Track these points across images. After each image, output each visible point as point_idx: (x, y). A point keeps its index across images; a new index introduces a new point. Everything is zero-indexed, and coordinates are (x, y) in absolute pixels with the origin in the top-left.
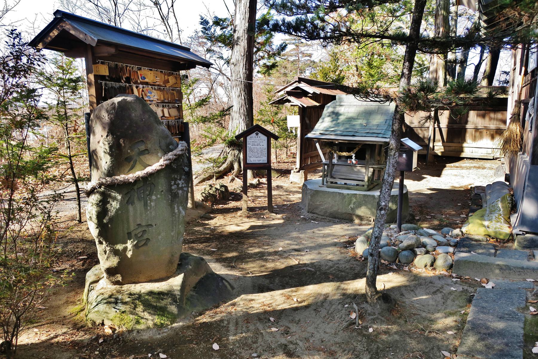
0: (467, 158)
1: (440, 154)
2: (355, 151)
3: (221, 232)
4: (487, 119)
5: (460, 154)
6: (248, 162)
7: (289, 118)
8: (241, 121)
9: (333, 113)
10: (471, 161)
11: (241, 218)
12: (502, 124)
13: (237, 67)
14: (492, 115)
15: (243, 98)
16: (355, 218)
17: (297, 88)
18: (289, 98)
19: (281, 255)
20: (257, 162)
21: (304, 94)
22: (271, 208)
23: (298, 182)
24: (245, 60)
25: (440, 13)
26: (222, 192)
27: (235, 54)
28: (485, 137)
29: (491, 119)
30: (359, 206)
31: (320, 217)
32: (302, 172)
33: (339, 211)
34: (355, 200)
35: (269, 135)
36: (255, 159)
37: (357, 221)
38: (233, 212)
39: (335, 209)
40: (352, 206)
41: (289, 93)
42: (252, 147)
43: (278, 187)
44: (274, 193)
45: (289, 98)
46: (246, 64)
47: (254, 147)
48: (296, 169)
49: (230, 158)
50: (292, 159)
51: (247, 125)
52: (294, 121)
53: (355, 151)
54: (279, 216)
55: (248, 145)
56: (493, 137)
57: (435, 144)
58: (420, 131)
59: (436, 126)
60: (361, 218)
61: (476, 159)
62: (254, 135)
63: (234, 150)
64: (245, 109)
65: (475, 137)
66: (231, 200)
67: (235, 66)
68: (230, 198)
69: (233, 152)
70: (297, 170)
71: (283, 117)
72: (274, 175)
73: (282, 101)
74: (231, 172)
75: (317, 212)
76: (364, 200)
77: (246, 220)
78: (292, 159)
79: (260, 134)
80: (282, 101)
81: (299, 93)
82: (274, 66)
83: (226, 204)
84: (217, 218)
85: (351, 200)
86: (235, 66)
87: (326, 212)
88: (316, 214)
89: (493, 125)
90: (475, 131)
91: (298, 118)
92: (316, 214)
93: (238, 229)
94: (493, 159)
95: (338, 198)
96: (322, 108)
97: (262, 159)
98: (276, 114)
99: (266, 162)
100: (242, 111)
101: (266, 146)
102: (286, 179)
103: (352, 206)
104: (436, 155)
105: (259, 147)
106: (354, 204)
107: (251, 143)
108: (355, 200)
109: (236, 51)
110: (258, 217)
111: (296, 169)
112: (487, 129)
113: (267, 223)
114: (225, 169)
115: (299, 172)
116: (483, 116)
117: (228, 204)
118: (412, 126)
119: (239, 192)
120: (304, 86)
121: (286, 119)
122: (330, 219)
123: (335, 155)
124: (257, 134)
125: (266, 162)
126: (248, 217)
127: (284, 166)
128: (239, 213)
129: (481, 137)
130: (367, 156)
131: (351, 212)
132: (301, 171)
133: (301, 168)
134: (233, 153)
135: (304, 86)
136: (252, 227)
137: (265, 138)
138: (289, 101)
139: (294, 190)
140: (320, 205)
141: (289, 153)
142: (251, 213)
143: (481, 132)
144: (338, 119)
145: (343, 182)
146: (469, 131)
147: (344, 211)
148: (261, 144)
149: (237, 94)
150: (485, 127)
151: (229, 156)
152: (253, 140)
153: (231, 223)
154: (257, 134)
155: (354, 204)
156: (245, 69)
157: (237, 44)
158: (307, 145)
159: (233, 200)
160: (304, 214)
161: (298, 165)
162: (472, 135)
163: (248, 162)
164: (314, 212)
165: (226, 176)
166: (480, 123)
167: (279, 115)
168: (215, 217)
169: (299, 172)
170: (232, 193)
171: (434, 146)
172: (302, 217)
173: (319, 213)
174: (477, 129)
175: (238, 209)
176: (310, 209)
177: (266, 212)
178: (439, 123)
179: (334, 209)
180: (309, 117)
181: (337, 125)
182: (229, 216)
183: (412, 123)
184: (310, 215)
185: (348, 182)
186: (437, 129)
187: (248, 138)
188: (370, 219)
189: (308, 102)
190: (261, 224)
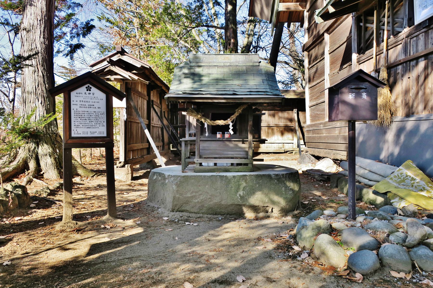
0: (263, 153)
2: (234, 117)
3: (30, 271)
4: (276, 117)
5: (258, 150)
6: (73, 135)
8: (38, 104)
10: (267, 155)
11: (65, 234)
12: (289, 122)
13: (31, 34)
14: (280, 114)
15: (40, 74)
16: (245, 209)
20: (89, 135)
22: (114, 210)
23: (124, 180)
24: (43, 26)
25: (230, 26)
26: (18, 196)
27: (29, 16)
28: (276, 134)
29: (280, 118)
30: (252, 192)
31: (193, 215)
32: (127, 166)
33: (223, 203)
34: (244, 184)
36: (86, 130)
37: (249, 214)
38: (44, 225)
39: (216, 200)
40: (241, 193)
42: (79, 109)
44: (201, 151)
46: (44, 32)
47: (83, 109)
48: (120, 163)
49: (22, 154)
53: (234, 117)
54: (130, 222)
55: (72, 107)
56: (282, 134)
60: (255, 209)
61: (271, 153)
62: (83, 89)
63: (27, 143)
64: (44, 89)
65: (268, 133)
66: (34, 208)
67: (28, 32)
68: (32, 205)
69: (27, 146)
70: (122, 164)
74: (24, 172)
75: (188, 208)
76: (258, 183)
79: (94, 89)
82: (79, 46)
83: (28, 215)
84: (15, 240)
85: (239, 185)
86: (28, 32)
87: (203, 206)
88: (186, 211)
89: (282, 123)
90: (268, 129)
92: (186, 211)
93: (67, 256)
94: (284, 153)
95: (219, 184)
97: (97, 130)
99: (105, 135)
100: (39, 92)
103: (241, 193)
105: (92, 110)
106: (243, 190)
107: (78, 103)
108: (244, 184)
109: (29, 14)
110: (98, 229)
111: (120, 163)
112: (277, 126)
113: (117, 236)
114: (14, 169)
116: (274, 116)
117: (31, 214)
119: (44, 195)
122: (209, 216)
124: (89, 89)
125: (105, 135)
126: (79, 230)
128: (58, 226)
129: (273, 133)
131: (241, 202)
132: (126, 166)
133: (126, 162)
134: (27, 147)
136: (94, 249)
139: (125, 188)
140: (192, 197)
142: (80, 223)
143: (273, 129)
145: (211, 163)
146: (263, 128)
147: (230, 202)
148: (96, 105)
150: (276, 124)
151: (20, 151)
152: (82, 99)
153: (48, 246)
154: (89, 89)
155: (243, 190)
156: (44, 38)
157: (31, 5)
159: (38, 207)
160: (166, 214)
162: (266, 132)
163: (73, 135)
164: (183, 209)
165: (17, 178)
166: (271, 121)
168: (10, 240)
169: (123, 166)
170: (34, 198)
172: (166, 218)
173: (192, 210)
174: (269, 127)
176: (176, 205)
177: (108, 219)
179: (215, 201)
182: (39, 233)
184: (178, 215)
185: (218, 161)
187: (73, 94)
188: (267, 208)
190: (107, 240)
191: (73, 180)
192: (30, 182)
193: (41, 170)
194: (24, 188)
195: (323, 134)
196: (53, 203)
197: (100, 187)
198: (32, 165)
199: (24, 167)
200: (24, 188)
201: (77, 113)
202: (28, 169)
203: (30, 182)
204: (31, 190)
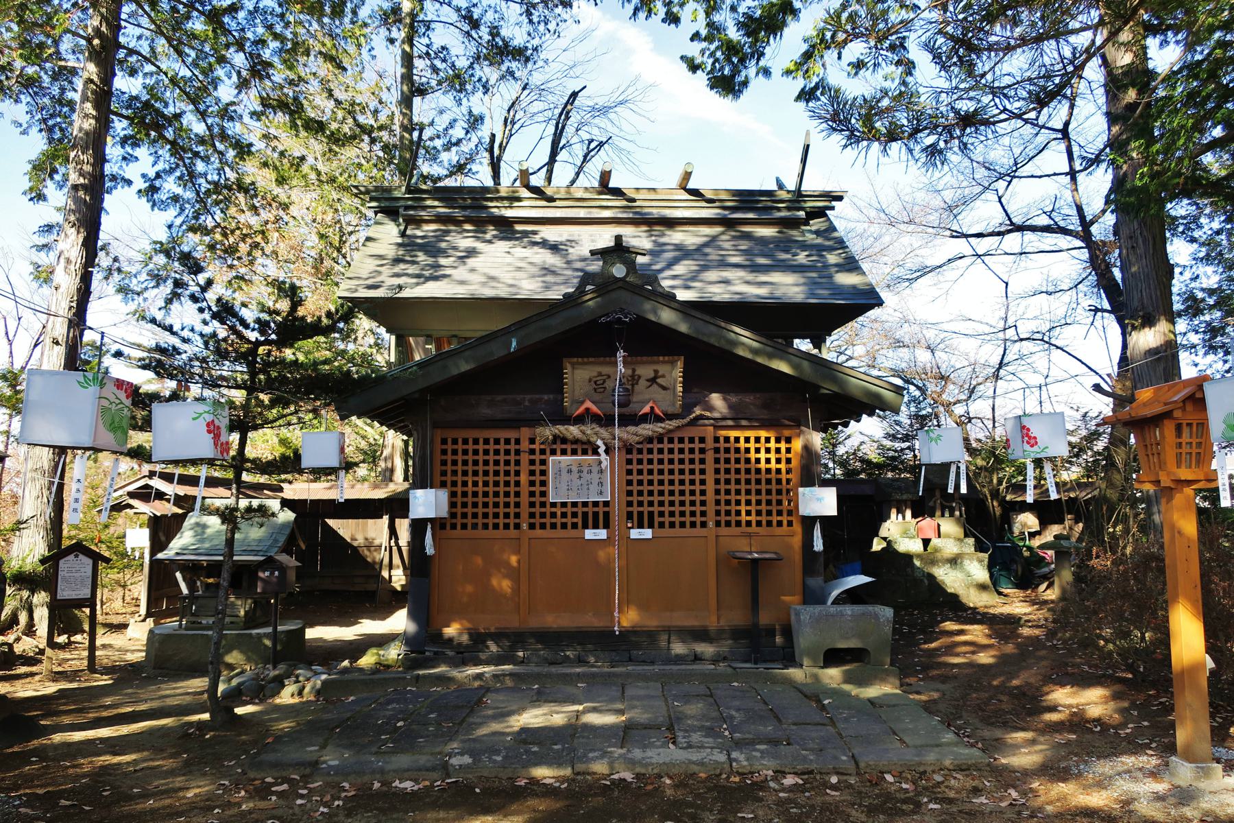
1: (399, 589)
7: (129, 532)
9: (197, 524)
17: (147, 486)
18: (132, 502)
19: (109, 707)
21: (160, 495)
35: (96, 558)
41: (132, 495)
43: (104, 646)
45: (132, 502)
50: (134, 609)
51: (50, 548)
52: (138, 539)
57: (393, 572)
58: (366, 553)
59: (393, 543)
62: (71, 557)
71: (120, 531)
72: (100, 631)
73: (118, 508)
77: (51, 684)
78: (134, 609)
79: (81, 556)
80: (118, 508)
81: (145, 494)
91: (146, 532)
96: (182, 518)
98: (106, 526)
101: (89, 573)
102: (121, 636)
104: (394, 591)
115: (144, 620)
118: (355, 544)
120: (157, 484)
121: (124, 536)
123: (199, 583)
124: (76, 556)
127: (116, 620)
128: (37, 678)
130: (245, 584)
135: (157, 484)
137: (90, 562)
138: (130, 507)
141: (128, 599)
144: (204, 533)
149: (35, 494)
154: (76, 556)
158: (160, 575)
159: (23, 665)
161: (143, 610)
167: (112, 529)
169: (144, 620)
170: (21, 657)
171: (390, 577)
175: (32, 675)
178: (397, 539)
180: (162, 529)
181: (202, 541)
183: (354, 539)
186: (395, 549)
187: (61, 562)
189: (169, 509)
191: (1169, 206)
192: (18, 639)
193: (33, 626)
194: (10, 646)
195: (610, 561)
196: (40, 661)
197: (957, 486)
198: (23, 618)
199: (14, 620)
200: (10, 646)
201: (64, 578)
202: (18, 624)
203: (18, 639)
204: (18, 649)
